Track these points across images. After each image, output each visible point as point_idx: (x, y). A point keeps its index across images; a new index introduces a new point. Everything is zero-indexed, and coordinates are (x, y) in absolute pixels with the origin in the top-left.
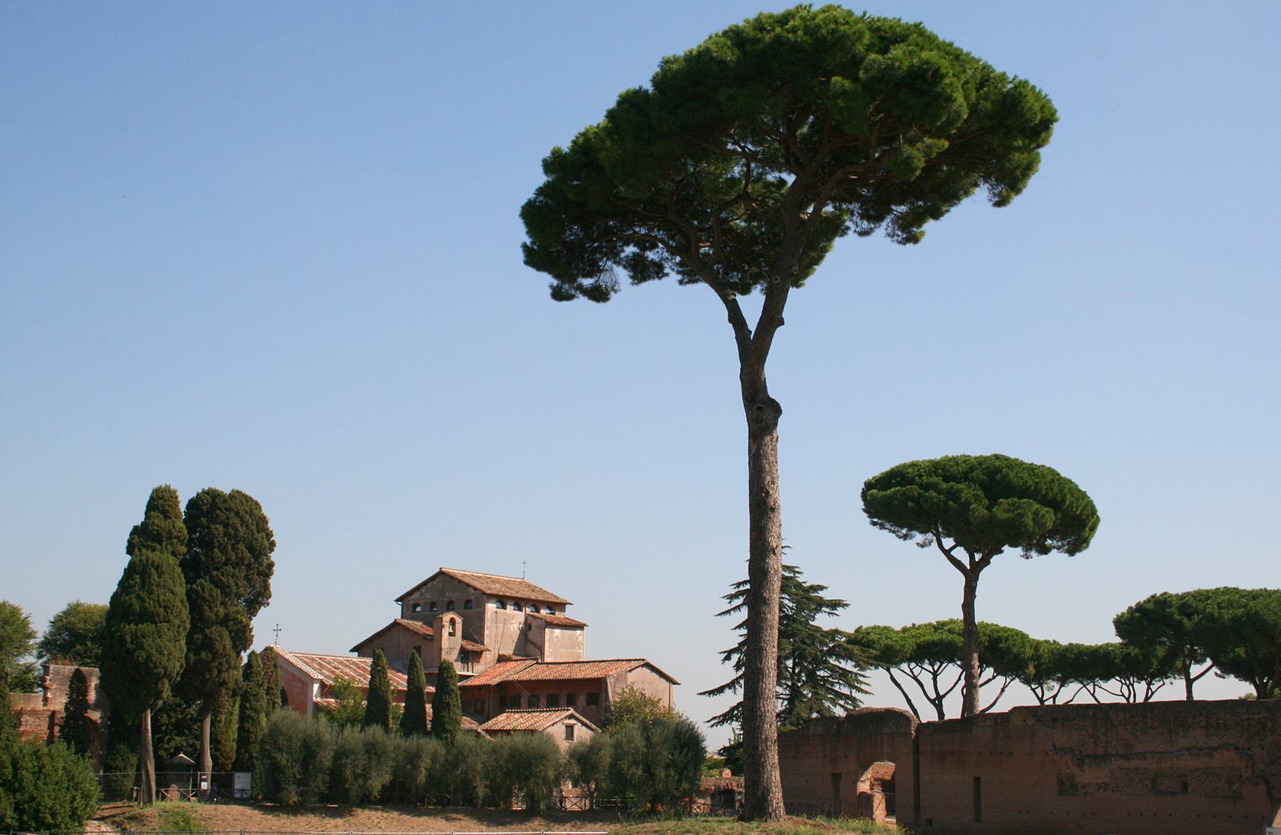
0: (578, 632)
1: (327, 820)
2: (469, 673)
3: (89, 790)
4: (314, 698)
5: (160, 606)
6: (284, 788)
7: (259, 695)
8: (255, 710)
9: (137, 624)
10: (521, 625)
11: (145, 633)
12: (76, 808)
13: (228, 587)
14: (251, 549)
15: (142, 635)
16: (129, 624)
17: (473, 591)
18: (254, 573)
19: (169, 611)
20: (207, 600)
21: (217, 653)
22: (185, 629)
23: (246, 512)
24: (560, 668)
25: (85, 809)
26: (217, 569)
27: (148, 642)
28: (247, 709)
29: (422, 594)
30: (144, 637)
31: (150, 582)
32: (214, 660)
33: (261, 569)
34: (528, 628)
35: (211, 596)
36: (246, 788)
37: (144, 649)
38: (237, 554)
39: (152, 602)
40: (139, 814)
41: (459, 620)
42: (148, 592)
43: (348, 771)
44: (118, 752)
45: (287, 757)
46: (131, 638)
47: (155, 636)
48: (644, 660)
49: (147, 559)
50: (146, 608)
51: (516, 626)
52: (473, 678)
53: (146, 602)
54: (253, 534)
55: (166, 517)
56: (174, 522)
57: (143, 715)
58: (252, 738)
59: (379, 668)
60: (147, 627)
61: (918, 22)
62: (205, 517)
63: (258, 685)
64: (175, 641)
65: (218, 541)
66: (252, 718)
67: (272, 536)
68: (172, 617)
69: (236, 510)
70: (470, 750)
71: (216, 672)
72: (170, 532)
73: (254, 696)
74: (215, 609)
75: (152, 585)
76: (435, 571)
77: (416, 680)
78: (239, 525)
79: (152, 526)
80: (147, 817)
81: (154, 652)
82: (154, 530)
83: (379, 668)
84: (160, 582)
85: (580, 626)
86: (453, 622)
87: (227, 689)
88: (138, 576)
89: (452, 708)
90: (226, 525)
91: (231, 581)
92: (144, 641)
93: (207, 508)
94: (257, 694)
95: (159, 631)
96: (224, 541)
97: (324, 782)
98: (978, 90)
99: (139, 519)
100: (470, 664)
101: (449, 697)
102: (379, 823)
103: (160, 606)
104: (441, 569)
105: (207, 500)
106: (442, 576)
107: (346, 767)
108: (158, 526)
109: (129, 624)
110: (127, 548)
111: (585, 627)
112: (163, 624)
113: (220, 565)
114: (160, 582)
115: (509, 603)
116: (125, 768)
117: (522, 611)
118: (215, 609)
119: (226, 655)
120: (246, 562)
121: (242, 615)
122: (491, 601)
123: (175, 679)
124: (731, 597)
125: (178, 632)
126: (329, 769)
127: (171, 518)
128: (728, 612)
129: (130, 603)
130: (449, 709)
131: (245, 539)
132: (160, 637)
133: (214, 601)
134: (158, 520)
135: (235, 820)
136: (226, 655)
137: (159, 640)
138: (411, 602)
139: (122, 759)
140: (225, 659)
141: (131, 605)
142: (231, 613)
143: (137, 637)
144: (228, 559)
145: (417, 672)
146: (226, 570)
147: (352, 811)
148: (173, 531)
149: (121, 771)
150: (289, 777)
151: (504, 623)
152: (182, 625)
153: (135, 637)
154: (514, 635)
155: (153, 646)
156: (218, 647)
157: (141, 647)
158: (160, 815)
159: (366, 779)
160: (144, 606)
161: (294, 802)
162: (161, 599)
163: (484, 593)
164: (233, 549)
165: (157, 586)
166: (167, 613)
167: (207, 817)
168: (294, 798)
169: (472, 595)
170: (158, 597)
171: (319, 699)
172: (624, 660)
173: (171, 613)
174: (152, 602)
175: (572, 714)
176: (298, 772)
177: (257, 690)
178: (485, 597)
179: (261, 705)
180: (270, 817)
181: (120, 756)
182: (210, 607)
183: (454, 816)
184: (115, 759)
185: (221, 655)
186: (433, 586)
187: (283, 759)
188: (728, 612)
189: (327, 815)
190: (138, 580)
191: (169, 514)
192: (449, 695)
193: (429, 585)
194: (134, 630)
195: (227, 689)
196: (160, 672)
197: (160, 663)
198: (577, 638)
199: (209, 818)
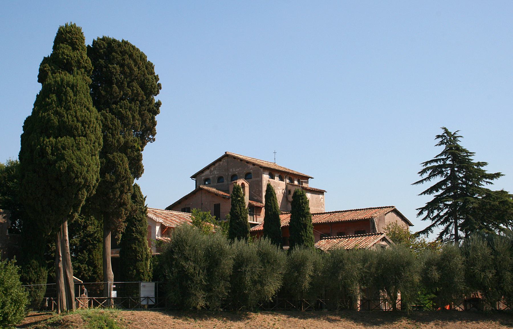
0: (321, 196)
1: (229, 323)
2: (255, 222)
3: (18, 296)
4: (157, 237)
5: (78, 121)
6: (193, 294)
7: (143, 221)
8: (141, 233)
9: (56, 137)
10: (284, 191)
11: (65, 145)
12: (7, 314)
13: (127, 118)
14: (143, 86)
15: (62, 147)
16: (48, 138)
17: (251, 166)
18: (145, 109)
19: (87, 126)
20: (110, 128)
21: (120, 175)
22: (99, 144)
23: (138, 57)
25: (15, 314)
26: (116, 103)
27: (68, 153)
28: (134, 232)
29: (211, 172)
30: (64, 148)
31: (67, 99)
32: (117, 181)
33: (151, 106)
34: (288, 193)
35: (113, 124)
36: (150, 296)
37: (65, 160)
38: (132, 90)
39: (70, 117)
40: (63, 320)
41: (247, 185)
42: (65, 108)
43: (248, 278)
44: (31, 266)
45: (193, 265)
46: (52, 150)
47: (75, 148)
48: (392, 207)
49: (62, 80)
50: (65, 122)
51: (281, 191)
52: (258, 225)
53: (64, 117)
54: (144, 75)
55: (74, 49)
56: (81, 53)
57: (62, 226)
58: (139, 256)
59: (239, 198)
60: (68, 140)
62: (102, 59)
63: (142, 212)
64: (92, 155)
65: (116, 79)
66: (137, 239)
67: (158, 79)
68: (89, 132)
69: (130, 53)
70: (348, 259)
71: (119, 193)
72: (78, 62)
73: (139, 221)
74: (117, 136)
75: (69, 102)
77: (273, 206)
78: (133, 65)
79: (62, 56)
80: (72, 322)
81: (75, 162)
82: (65, 58)
83: (239, 198)
84: (76, 100)
85: (321, 192)
87: (126, 209)
88: (54, 95)
89: (308, 228)
90: (122, 66)
91: (129, 113)
92: (65, 152)
93: (104, 52)
94: (141, 220)
95: (79, 144)
96: (121, 78)
97: (226, 288)
99: (49, 52)
100: (254, 216)
101: (305, 219)
102: (274, 324)
103: (78, 121)
104: (226, 152)
105: (104, 45)
106: (226, 158)
107: (245, 274)
108: (67, 56)
109: (48, 138)
110: (39, 76)
111: (325, 193)
112: (81, 137)
113: (118, 99)
114: (76, 100)
115: (277, 175)
116: (38, 280)
117: (284, 181)
118: (117, 136)
119: (127, 178)
120: (140, 98)
121: (138, 144)
122: (265, 173)
123: (92, 192)
125: (94, 146)
126: (230, 276)
127: (79, 50)
128: (422, 181)
129: (49, 118)
130: (306, 229)
131: (138, 79)
132: (79, 149)
133: (116, 130)
134: (66, 50)
135: (152, 324)
136: (127, 178)
137: (78, 153)
139: (35, 273)
140: (126, 181)
141: (49, 120)
142: (130, 141)
143: (57, 149)
144: (126, 94)
145: (273, 200)
146: (124, 103)
147: (247, 315)
148: (82, 61)
149: (34, 283)
150: (197, 283)
152: (97, 141)
153: (55, 149)
154: (280, 197)
155: (74, 157)
156: (121, 170)
157: (62, 158)
158: (85, 321)
159: (263, 285)
160: (62, 120)
161: (202, 307)
162: (78, 114)
163: (261, 167)
164: (128, 87)
165: (74, 103)
166: (85, 128)
167: (126, 321)
168: (201, 303)
169: (251, 169)
170: (76, 112)
171: (160, 238)
172: (376, 208)
173: (88, 128)
174: (70, 117)
175: (384, 237)
176: (204, 278)
177: (142, 216)
178: (262, 170)
179: (145, 229)
180: (181, 321)
181: (33, 269)
182: (113, 134)
183: (334, 318)
184: (28, 272)
185: (123, 177)
186: (220, 165)
187: (189, 266)
188: (422, 181)
189: (228, 319)
190: (55, 98)
191: (77, 46)
192: (305, 217)
193: (217, 165)
194: (54, 142)
195: (126, 209)
196: (81, 182)
197: (81, 174)
198: (321, 200)
199: (129, 323)
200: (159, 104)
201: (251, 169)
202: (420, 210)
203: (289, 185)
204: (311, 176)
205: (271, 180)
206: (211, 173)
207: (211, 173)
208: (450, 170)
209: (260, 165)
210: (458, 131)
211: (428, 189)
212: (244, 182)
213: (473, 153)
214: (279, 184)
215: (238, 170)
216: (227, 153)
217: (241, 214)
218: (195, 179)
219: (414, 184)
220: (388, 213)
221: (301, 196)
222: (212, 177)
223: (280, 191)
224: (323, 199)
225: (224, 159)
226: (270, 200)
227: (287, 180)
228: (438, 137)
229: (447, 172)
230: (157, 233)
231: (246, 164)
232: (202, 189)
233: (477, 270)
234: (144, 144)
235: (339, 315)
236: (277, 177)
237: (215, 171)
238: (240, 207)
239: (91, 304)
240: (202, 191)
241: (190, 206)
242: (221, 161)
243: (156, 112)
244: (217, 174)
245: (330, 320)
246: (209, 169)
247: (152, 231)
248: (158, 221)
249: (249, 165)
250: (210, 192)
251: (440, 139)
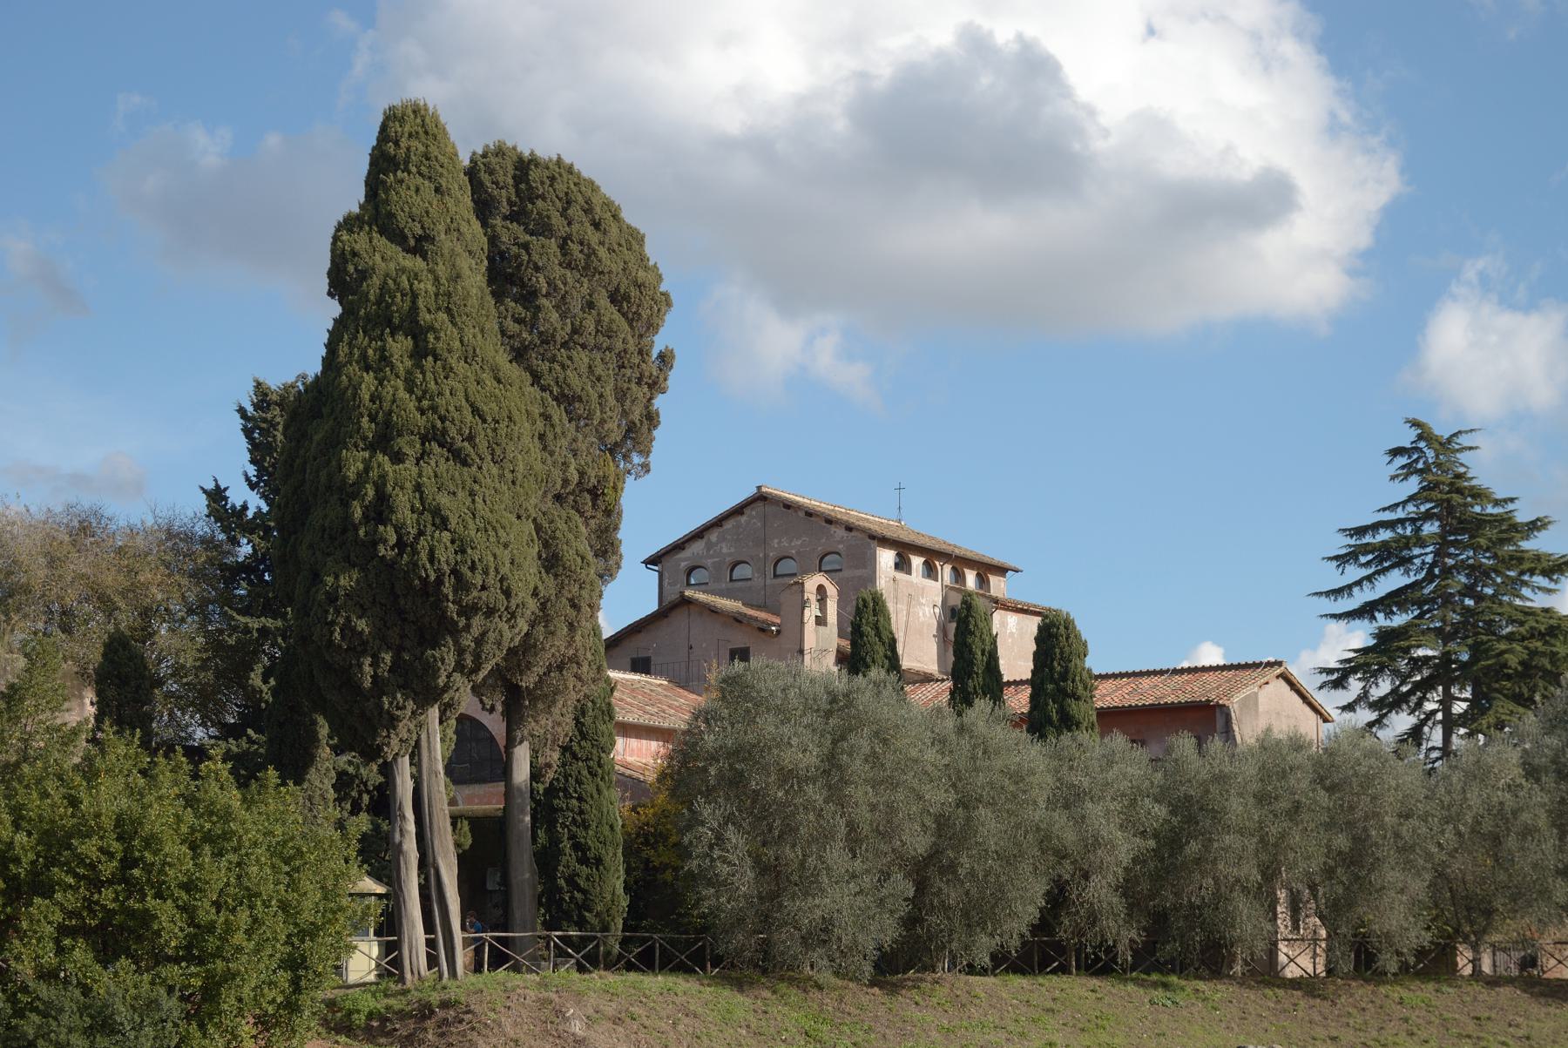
17: (840, 532)
24: (1146, 682)
29: (709, 546)
41: (832, 591)
51: (928, 610)
61: (238, 422)
76: (746, 492)
86: (821, 589)
98: (411, 392)
104: (759, 488)
106: (760, 504)
124: (1342, 560)
138: (683, 564)
151: (909, 605)
163: (873, 537)
193: (729, 525)
200: (665, 359)
201: (840, 542)
206: (708, 550)
207: (708, 550)
208: (1432, 552)
209: (870, 529)
210: (1460, 432)
213: (1512, 500)
214: (923, 589)
215: (799, 542)
216: (764, 490)
218: (656, 568)
222: (714, 563)
223: (927, 609)
225: (752, 510)
228: (1396, 452)
229: (1423, 560)
231: (824, 524)
232: (685, 602)
237: (724, 545)
239: (482, 966)
240: (691, 607)
241: (649, 653)
242: (742, 514)
243: (656, 385)
244: (730, 554)
246: (702, 538)
249: (833, 528)
250: (716, 612)
251: (1402, 460)
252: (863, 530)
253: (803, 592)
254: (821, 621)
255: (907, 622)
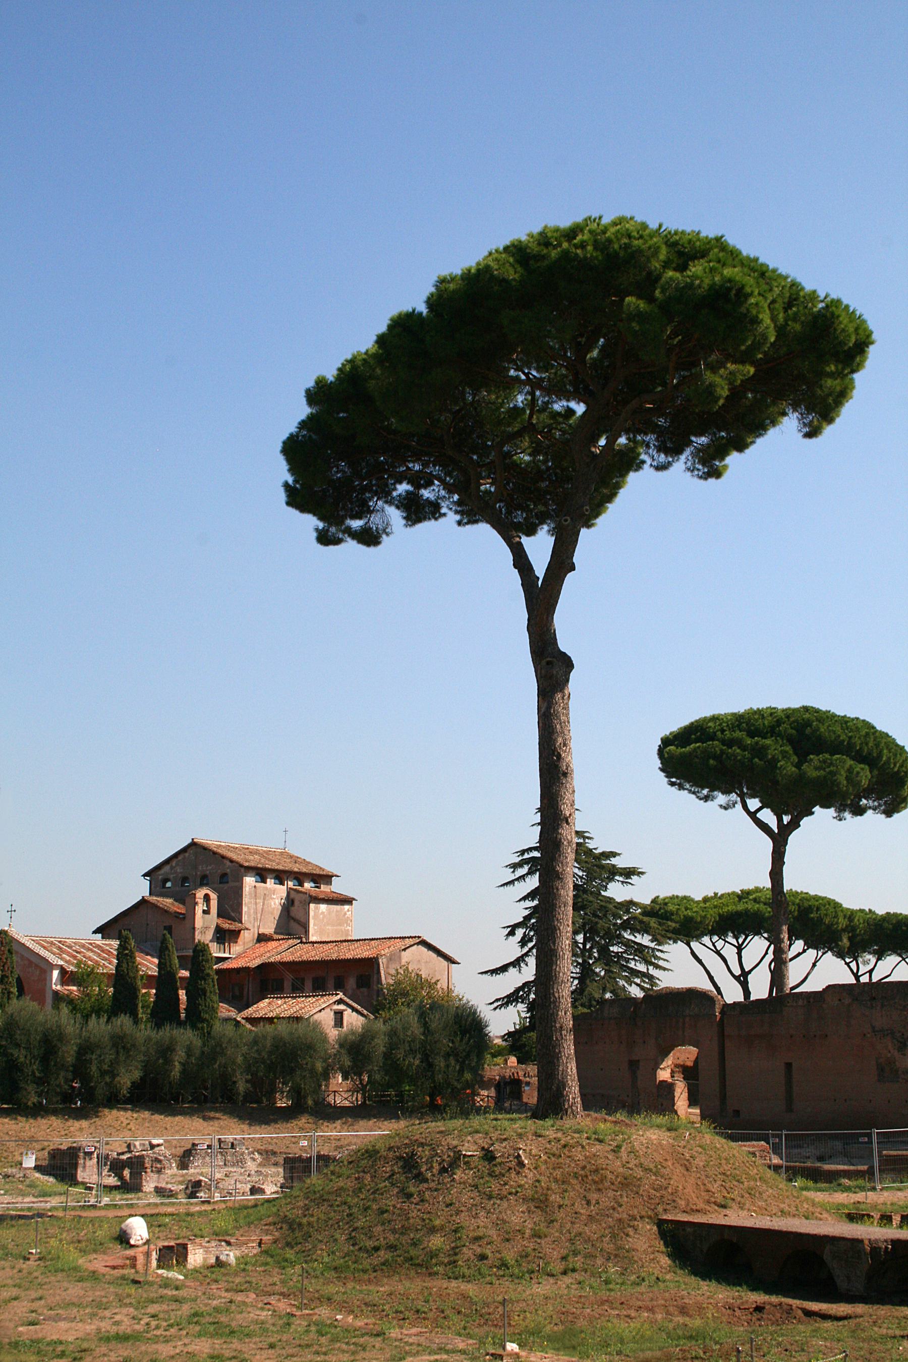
0: (346, 907)
2: (227, 955)
4: (54, 986)
10: (283, 901)
17: (228, 863)
29: (172, 868)
41: (214, 897)
43: (94, 1068)
48: (419, 937)
51: (277, 902)
52: (230, 960)
59: (127, 952)
77: (168, 964)
83: (127, 952)
85: (348, 901)
86: (207, 898)
89: (208, 994)
100: (226, 944)
101: (205, 983)
104: (193, 839)
106: (193, 847)
117: (284, 885)
122: (249, 875)
124: (515, 866)
126: (73, 1066)
128: (512, 882)
130: (205, 996)
138: (160, 877)
145: (169, 955)
147: (98, 1112)
154: (275, 912)
159: (114, 1076)
161: (34, 1103)
168: (33, 1099)
171: (59, 987)
172: (397, 938)
175: (341, 999)
178: (243, 870)
180: (6, 1120)
183: (212, 1114)
187: (20, 1055)
188: (512, 882)
193: (180, 858)
198: (345, 914)
202: (509, 929)
203: (292, 892)
204: (335, 873)
205: (258, 885)
211: (528, 894)
212: (208, 892)
214: (274, 891)
217: (128, 973)
219: (501, 886)
220: (408, 947)
221: (202, 951)
224: (350, 913)
226: (165, 955)
227: (289, 883)
230: (54, 981)
233: (400, 1054)
234: (712, 239)
235: (221, 1111)
236: (271, 879)
237: (178, 867)
238: (127, 963)
244: (181, 873)
245: (205, 1118)
247: (48, 978)
248: (55, 962)
249: (225, 861)
252: (237, 863)
253: (195, 898)
254: (205, 912)
255: (262, 909)
